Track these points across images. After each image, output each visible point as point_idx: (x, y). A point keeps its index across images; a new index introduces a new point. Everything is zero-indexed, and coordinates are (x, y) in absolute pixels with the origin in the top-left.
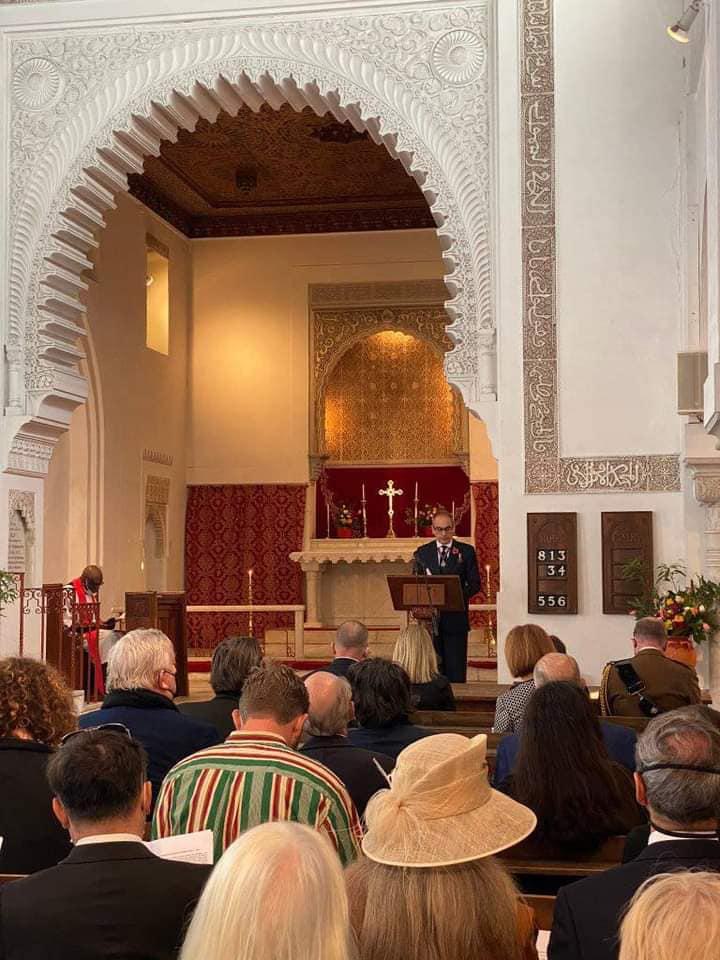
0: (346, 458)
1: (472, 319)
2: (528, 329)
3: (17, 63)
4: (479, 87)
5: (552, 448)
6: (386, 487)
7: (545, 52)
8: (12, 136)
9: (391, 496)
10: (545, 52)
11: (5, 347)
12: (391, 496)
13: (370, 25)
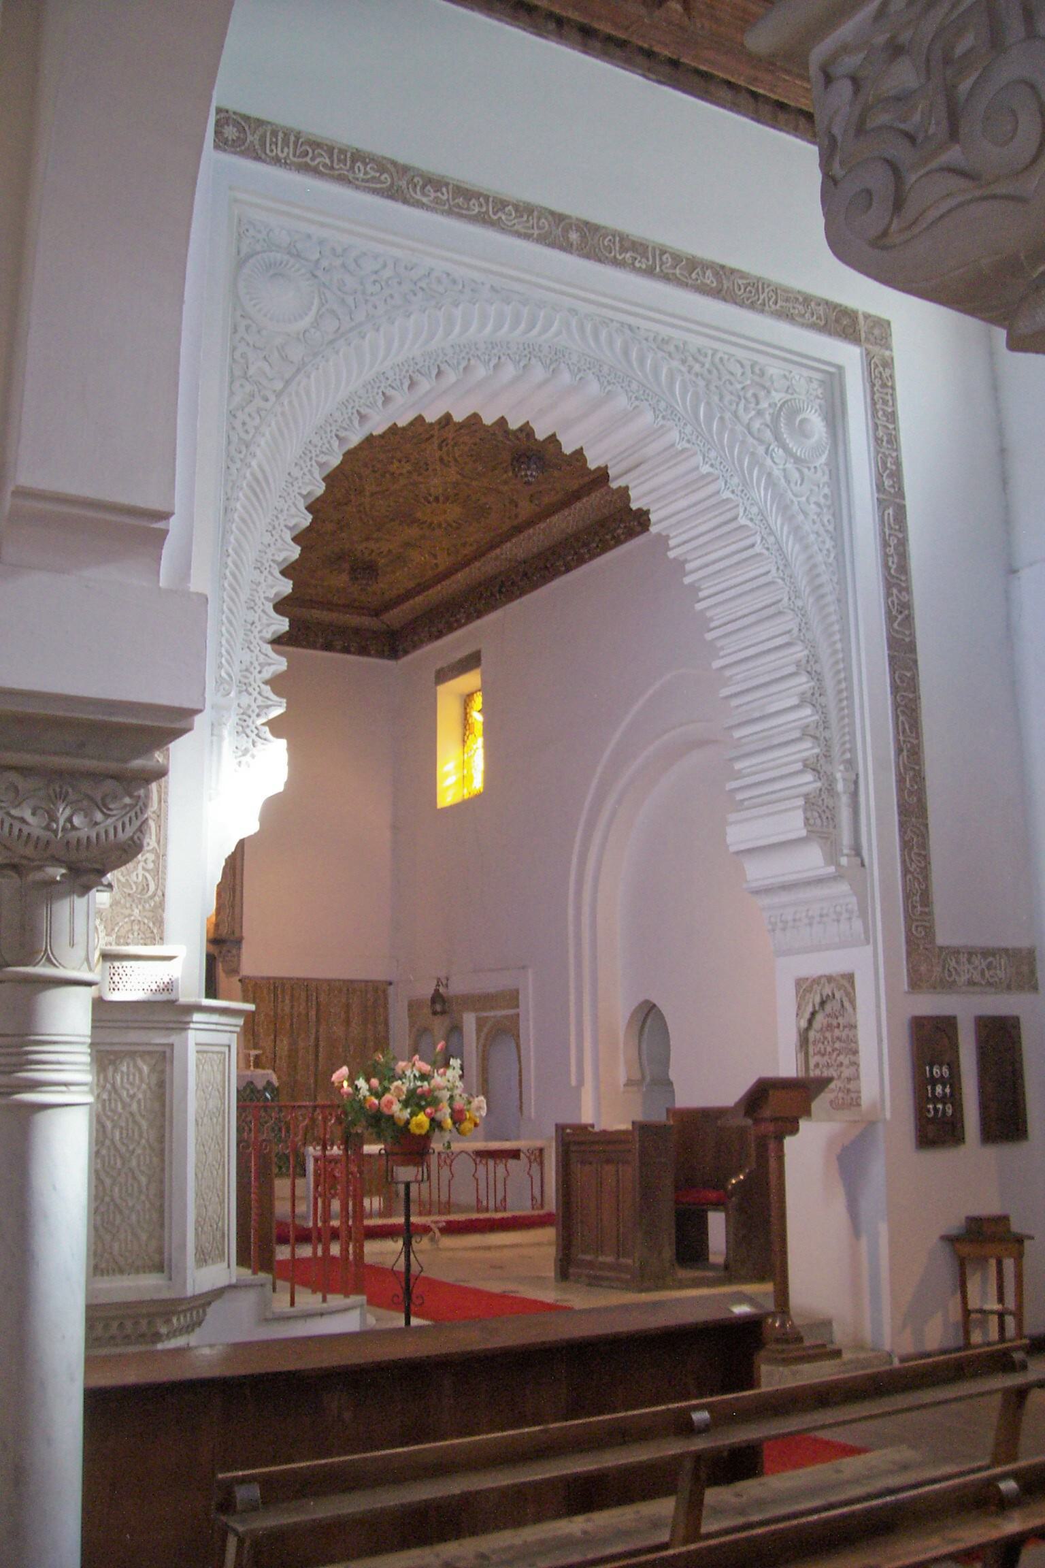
5: (929, 932)
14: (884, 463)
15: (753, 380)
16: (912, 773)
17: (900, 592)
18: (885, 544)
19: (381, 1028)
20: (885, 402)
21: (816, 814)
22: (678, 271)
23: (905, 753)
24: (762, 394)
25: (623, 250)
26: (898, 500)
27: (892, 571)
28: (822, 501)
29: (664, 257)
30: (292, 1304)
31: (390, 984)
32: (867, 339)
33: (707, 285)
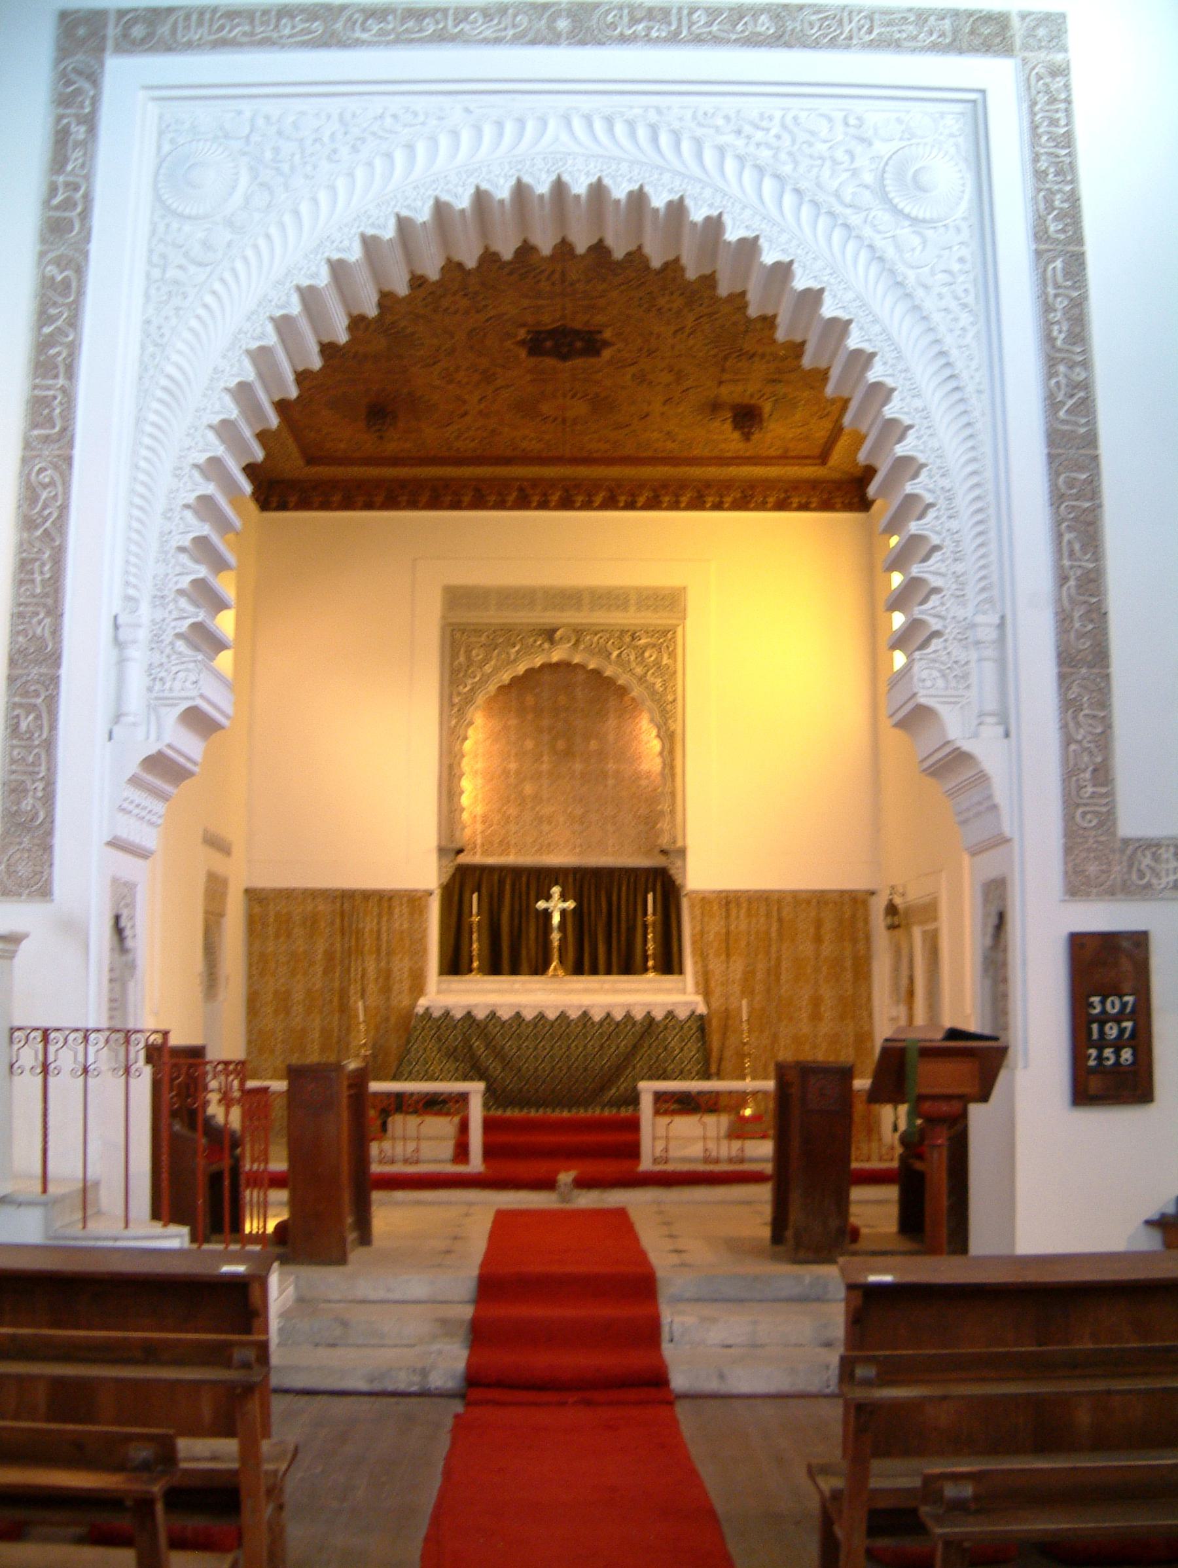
0: (485, 853)
1: (960, 597)
2: (1063, 620)
3: (167, 147)
4: (958, 230)
5: (1107, 820)
6: (564, 897)
7: (1068, 188)
8: (150, 262)
9: (550, 905)
10: (1068, 188)
11: (116, 617)
12: (550, 905)
13: (777, 120)
14: (1049, 203)
15: (846, 134)
16: (1082, 609)
17: (1071, 368)
18: (1047, 307)
19: (861, 946)
20: (1054, 122)
21: (936, 674)
22: (715, 28)
23: (1072, 583)
24: (859, 149)
25: (634, 21)
26: (1071, 248)
27: (1059, 343)
28: (956, 267)
29: (695, 16)
30: (45, 1190)
31: (873, 893)
32: (1026, 47)
33: (760, 34)
